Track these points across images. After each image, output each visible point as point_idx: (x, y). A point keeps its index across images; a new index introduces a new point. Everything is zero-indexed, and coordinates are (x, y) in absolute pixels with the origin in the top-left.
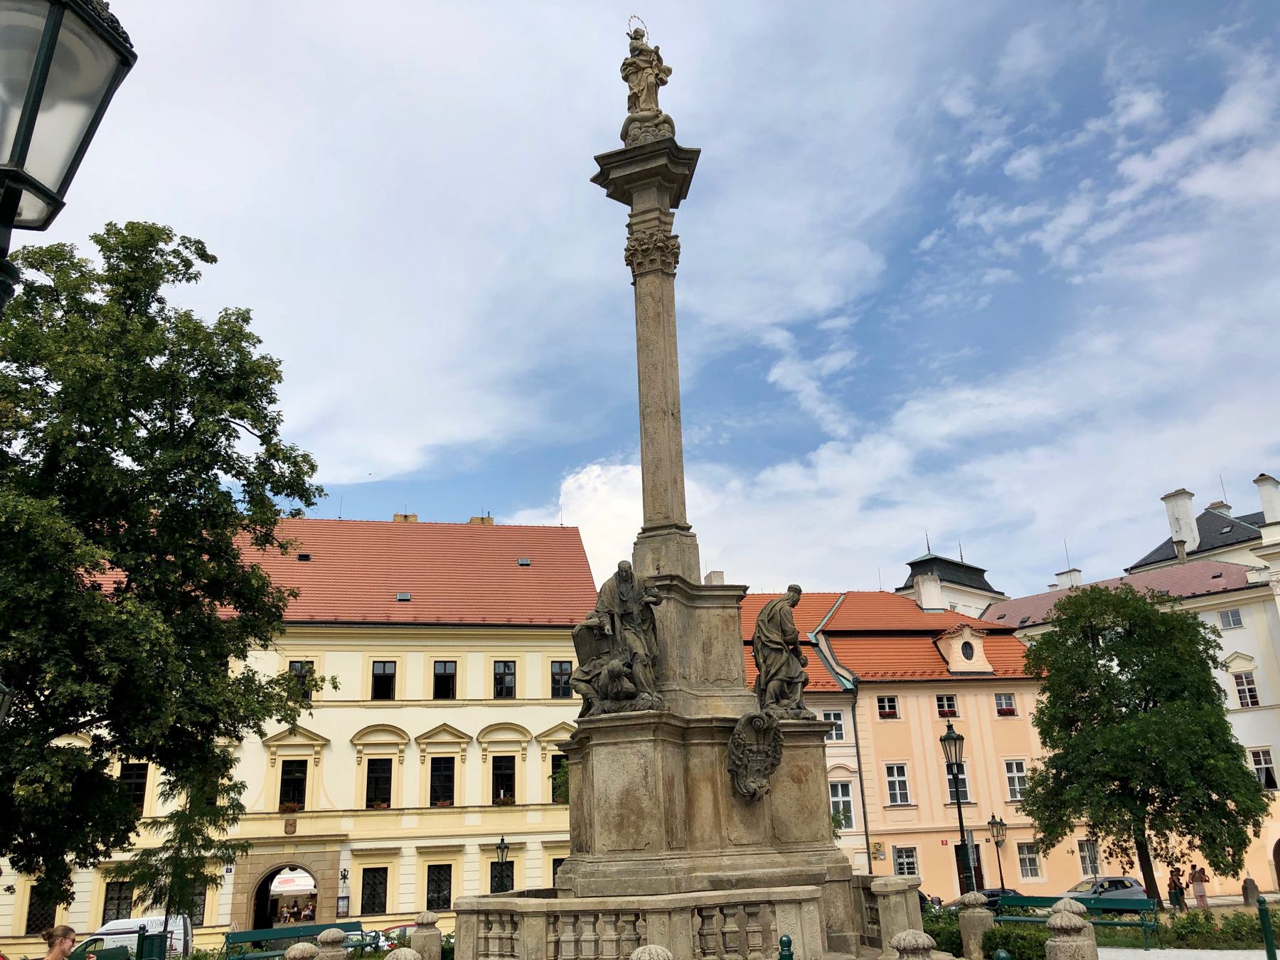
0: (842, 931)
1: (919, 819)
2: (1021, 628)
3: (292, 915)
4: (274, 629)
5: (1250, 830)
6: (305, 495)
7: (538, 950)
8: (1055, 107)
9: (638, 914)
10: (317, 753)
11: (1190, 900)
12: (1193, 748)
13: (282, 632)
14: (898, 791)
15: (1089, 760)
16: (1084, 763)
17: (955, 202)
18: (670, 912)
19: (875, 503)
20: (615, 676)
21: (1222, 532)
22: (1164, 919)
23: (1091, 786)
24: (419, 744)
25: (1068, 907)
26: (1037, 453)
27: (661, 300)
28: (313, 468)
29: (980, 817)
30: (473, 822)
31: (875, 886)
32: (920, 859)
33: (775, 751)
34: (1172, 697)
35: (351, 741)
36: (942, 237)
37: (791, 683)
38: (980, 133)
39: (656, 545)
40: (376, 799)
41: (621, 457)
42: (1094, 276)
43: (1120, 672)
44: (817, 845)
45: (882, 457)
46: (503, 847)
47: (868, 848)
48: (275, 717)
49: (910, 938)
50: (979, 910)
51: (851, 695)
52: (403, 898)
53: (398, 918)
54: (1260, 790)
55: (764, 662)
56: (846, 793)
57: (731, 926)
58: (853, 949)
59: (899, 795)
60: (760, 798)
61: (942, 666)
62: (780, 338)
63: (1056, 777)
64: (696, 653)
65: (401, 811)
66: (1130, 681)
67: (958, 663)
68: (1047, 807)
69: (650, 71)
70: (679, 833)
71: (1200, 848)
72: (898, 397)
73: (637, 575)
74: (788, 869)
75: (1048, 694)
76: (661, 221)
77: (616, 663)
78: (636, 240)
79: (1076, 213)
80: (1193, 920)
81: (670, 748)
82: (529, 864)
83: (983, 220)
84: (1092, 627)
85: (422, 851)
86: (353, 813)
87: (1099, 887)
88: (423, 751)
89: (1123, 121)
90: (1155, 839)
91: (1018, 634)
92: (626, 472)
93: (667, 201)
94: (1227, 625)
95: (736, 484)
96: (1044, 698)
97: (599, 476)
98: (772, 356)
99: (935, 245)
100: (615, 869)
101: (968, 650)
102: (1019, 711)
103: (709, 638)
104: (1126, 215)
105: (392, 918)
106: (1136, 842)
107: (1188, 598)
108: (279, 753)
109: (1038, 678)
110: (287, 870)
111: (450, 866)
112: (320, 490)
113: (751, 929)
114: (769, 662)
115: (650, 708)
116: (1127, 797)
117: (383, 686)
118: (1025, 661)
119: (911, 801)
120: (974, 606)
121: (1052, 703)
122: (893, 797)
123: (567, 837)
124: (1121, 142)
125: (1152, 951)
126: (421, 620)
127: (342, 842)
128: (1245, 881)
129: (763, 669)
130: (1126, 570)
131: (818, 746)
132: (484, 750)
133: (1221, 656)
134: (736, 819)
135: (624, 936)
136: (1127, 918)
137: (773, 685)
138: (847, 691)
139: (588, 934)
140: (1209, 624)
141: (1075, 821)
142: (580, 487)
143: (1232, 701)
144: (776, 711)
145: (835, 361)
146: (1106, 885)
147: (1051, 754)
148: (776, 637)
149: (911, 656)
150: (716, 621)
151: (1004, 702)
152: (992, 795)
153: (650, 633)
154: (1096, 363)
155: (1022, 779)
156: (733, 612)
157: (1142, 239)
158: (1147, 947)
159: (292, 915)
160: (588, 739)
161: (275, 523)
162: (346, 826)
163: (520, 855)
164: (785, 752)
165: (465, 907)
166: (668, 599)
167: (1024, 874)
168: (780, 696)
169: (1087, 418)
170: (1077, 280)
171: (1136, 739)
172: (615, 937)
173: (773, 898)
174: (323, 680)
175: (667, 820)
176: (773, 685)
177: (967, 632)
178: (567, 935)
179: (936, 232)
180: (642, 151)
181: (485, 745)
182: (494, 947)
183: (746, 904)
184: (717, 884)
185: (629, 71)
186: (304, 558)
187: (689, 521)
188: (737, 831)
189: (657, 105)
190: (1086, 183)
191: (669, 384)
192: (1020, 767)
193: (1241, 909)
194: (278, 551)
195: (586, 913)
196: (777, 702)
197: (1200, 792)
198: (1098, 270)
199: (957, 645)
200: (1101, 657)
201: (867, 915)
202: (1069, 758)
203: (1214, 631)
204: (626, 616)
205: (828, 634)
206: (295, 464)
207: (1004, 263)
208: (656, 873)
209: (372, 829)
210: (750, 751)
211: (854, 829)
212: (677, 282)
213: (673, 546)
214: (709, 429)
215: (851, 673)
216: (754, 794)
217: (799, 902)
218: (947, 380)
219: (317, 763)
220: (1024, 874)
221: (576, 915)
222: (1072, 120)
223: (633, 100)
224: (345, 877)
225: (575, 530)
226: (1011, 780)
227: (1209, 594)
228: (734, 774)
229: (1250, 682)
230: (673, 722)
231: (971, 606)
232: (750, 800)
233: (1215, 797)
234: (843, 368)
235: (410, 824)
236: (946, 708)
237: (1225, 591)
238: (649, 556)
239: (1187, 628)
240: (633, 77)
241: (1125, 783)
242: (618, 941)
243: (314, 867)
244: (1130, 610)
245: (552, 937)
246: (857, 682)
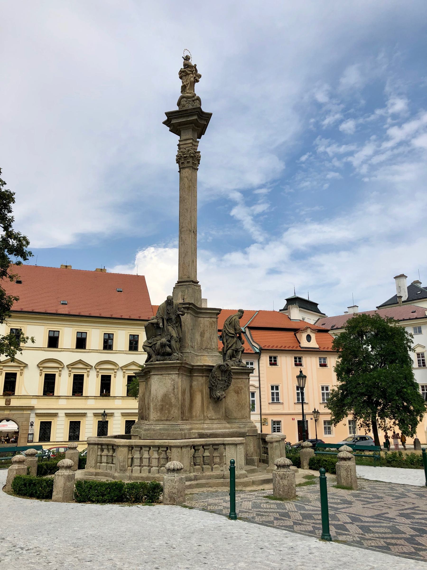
0: (252, 456)
1: (283, 409)
2: (332, 329)
3: (6, 440)
4: (6, 315)
5: (418, 418)
6: (24, 255)
7: (124, 461)
8: (363, 102)
9: (168, 448)
10: (22, 370)
11: (392, 446)
12: (398, 384)
13: (10, 316)
14: (275, 397)
15: (356, 387)
16: (354, 388)
17: (317, 141)
18: (181, 447)
19: (273, 271)
20: (163, 345)
21: (417, 293)
22: (382, 454)
23: (356, 398)
24: (68, 368)
25: (345, 449)
26: (344, 254)
27: (191, 180)
28: (28, 243)
29: (309, 409)
30: (91, 402)
31: (268, 439)
32: (283, 426)
33: (229, 380)
34: (392, 362)
35: (38, 365)
36: (310, 156)
37: (237, 351)
38: (330, 111)
39: (183, 289)
40: (47, 392)
41: (164, 244)
42: (373, 179)
43: (371, 351)
44: (243, 420)
45: (277, 252)
47: (261, 420)
48: (5, 354)
49: (282, 461)
50: (309, 449)
51: (258, 355)
52: (58, 435)
53: (55, 443)
54: (423, 402)
55: (226, 341)
57: (207, 454)
58: (256, 464)
59: (275, 398)
60: (222, 399)
61: (296, 344)
62: (237, 196)
63: (342, 394)
64: (198, 337)
66: (376, 355)
67: (304, 343)
68: (337, 406)
69: (192, 75)
70: (186, 413)
71: (398, 425)
72: (285, 226)
73: (175, 302)
74: (231, 430)
75: (341, 359)
76: (193, 144)
77: (164, 340)
78: (182, 152)
79: (368, 150)
80: (394, 455)
81: (185, 377)
82: (115, 422)
83: (328, 150)
84: (362, 331)
86: (37, 397)
87: (356, 439)
88: (70, 371)
89: (391, 111)
90: (380, 420)
91: (330, 332)
92: (165, 251)
93: (196, 136)
94: (416, 333)
95: (213, 260)
96: (340, 360)
97: (153, 252)
98: (233, 204)
99: (307, 159)
100: (158, 428)
101: (309, 338)
102: (328, 365)
103: (204, 331)
104: (389, 153)
105: (53, 443)
106: (372, 422)
107: (401, 320)
108: (4, 369)
109: (338, 351)
110: (5, 421)
112: (30, 253)
113: (215, 455)
114: (228, 342)
115: (177, 360)
116: (371, 404)
117: (53, 342)
118: (333, 344)
120: (312, 319)
121: (343, 362)
122: (273, 399)
123: (137, 411)
124: (389, 120)
125: (377, 467)
126: (71, 313)
127: (31, 409)
128: (415, 439)
129: (226, 344)
130: (377, 307)
131: (246, 378)
132: (98, 372)
133: (412, 346)
134: (211, 408)
135: (162, 456)
136: (367, 453)
137: (229, 351)
138: (256, 353)
139: (146, 455)
140: (409, 332)
141: (348, 412)
142: (145, 257)
143: (415, 365)
144: (230, 363)
145: (260, 208)
146: (358, 439)
147: (341, 384)
148: (232, 331)
149: (285, 339)
150: (207, 323)
151: (322, 361)
152: (315, 400)
153: (179, 328)
154: (371, 218)
155: (327, 394)
156: (215, 320)
157: (395, 164)
158: (375, 466)
159: (6, 440)
160: (149, 372)
161: (8, 267)
162: (34, 403)
163: (111, 418)
164: (233, 380)
165: (92, 442)
166: (187, 313)
167: (326, 433)
168: (232, 356)
169: (366, 240)
170: (366, 180)
171: (376, 379)
172: (157, 457)
173: (225, 442)
174: (28, 338)
175: (182, 408)
176: (229, 351)
178: (137, 455)
179: (308, 154)
180: (186, 112)
181: (98, 370)
182: (104, 459)
183: (213, 445)
184: (201, 436)
185: (183, 74)
186: (19, 282)
187: (198, 280)
188: (211, 413)
189: (194, 91)
190: (373, 137)
191: (193, 218)
192: (327, 389)
193: (414, 451)
194: (9, 279)
195: (145, 446)
196: (231, 359)
197: (400, 402)
198: (376, 176)
199: (304, 336)
200: (364, 344)
201: (262, 450)
202: (348, 386)
203: (411, 335)
204: (169, 320)
206: (20, 241)
207: (335, 169)
208: (176, 430)
209: (46, 404)
210: (219, 379)
211: (256, 412)
212: (199, 173)
213: (190, 290)
214: (203, 234)
215: (259, 345)
216: (219, 398)
217: (236, 445)
218: (307, 220)
219: (21, 374)
220: (326, 433)
221: (141, 447)
222: (369, 110)
223: (184, 88)
224: (32, 425)
225: (143, 278)
226: (323, 394)
227: (410, 319)
228: (211, 389)
229: (423, 357)
230: (187, 366)
231: (311, 319)
232: (217, 400)
233: (405, 404)
234: (264, 211)
235: (62, 403)
236: (298, 362)
237: (416, 318)
238: (180, 294)
239: (400, 333)
240: (184, 78)
241: (369, 398)
242: (159, 459)
243: (18, 420)
244: (378, 325)
245: (130, 456)
246: (261, 349)
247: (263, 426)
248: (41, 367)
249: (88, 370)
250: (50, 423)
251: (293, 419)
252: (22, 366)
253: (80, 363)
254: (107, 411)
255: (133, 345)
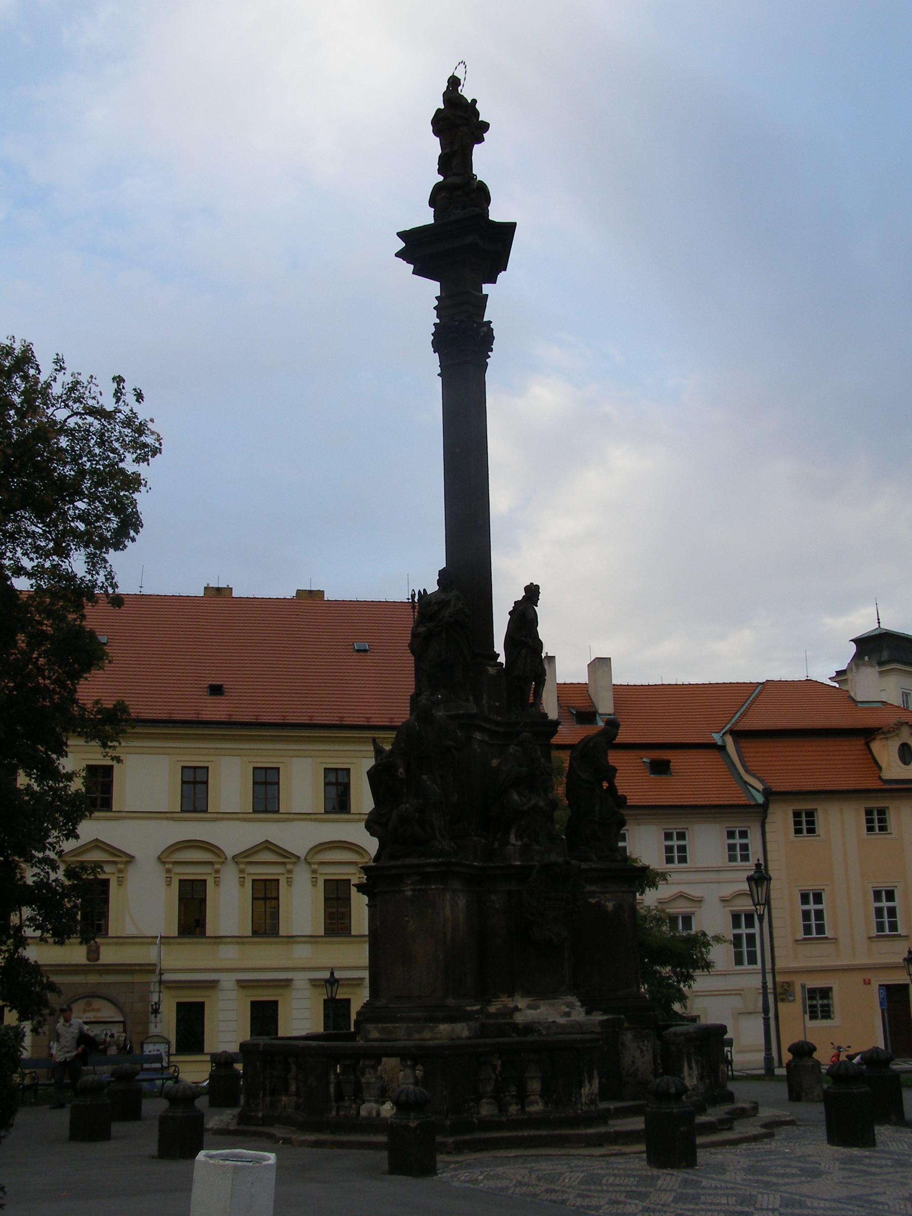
10: (120, 871)
32: (837, 1001)
35: (159, 858)
46: (332, 982)
51: (761, 812)
56: (750, 924)
59: (814, 925)
65: (291, 939)
85: (243, 985)
88: (242, 871)
111: (276, 1002)
119: (828, 933)
122: (807, 930)
138: (758, 805)
177: (905, 731)
205: (737, 735)
209: (184, 960)
224: (156, 1011)
235: (229, 954)
246: (768, 793)
247: (780, 1005)
248: (169, 863)
249: (289, 867)
250: (276, 1003)
251: (867, 982)
252: (121, 863)
253: (97, 847)
254: (337, 975)
255: (338, 798)
